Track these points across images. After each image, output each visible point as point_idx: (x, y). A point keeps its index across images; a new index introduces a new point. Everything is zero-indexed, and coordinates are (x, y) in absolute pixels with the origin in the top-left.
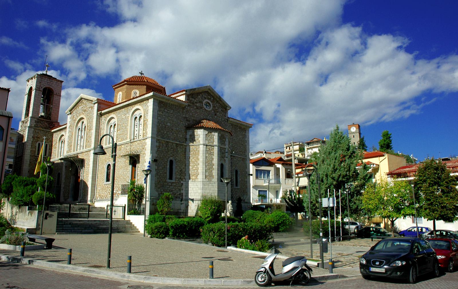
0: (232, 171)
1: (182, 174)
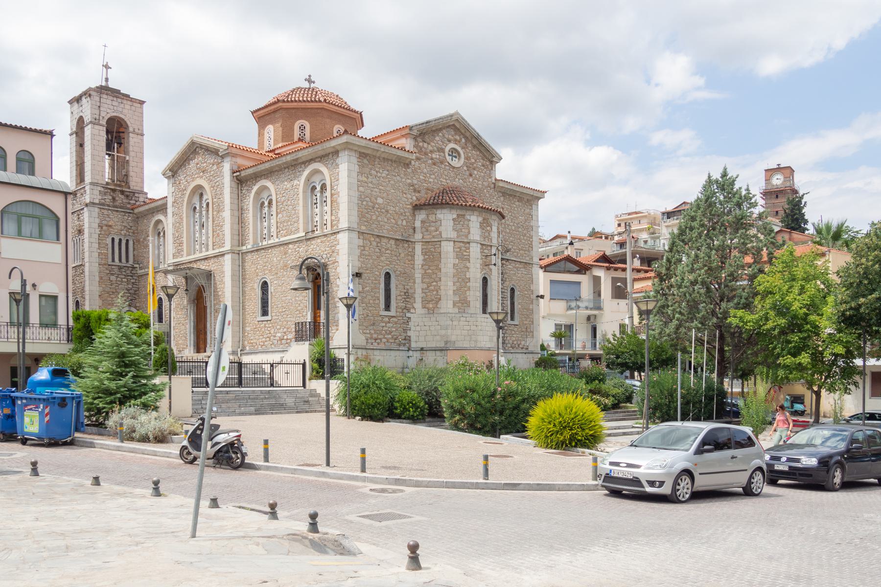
0: (503, 290)
1: (408, 300)
